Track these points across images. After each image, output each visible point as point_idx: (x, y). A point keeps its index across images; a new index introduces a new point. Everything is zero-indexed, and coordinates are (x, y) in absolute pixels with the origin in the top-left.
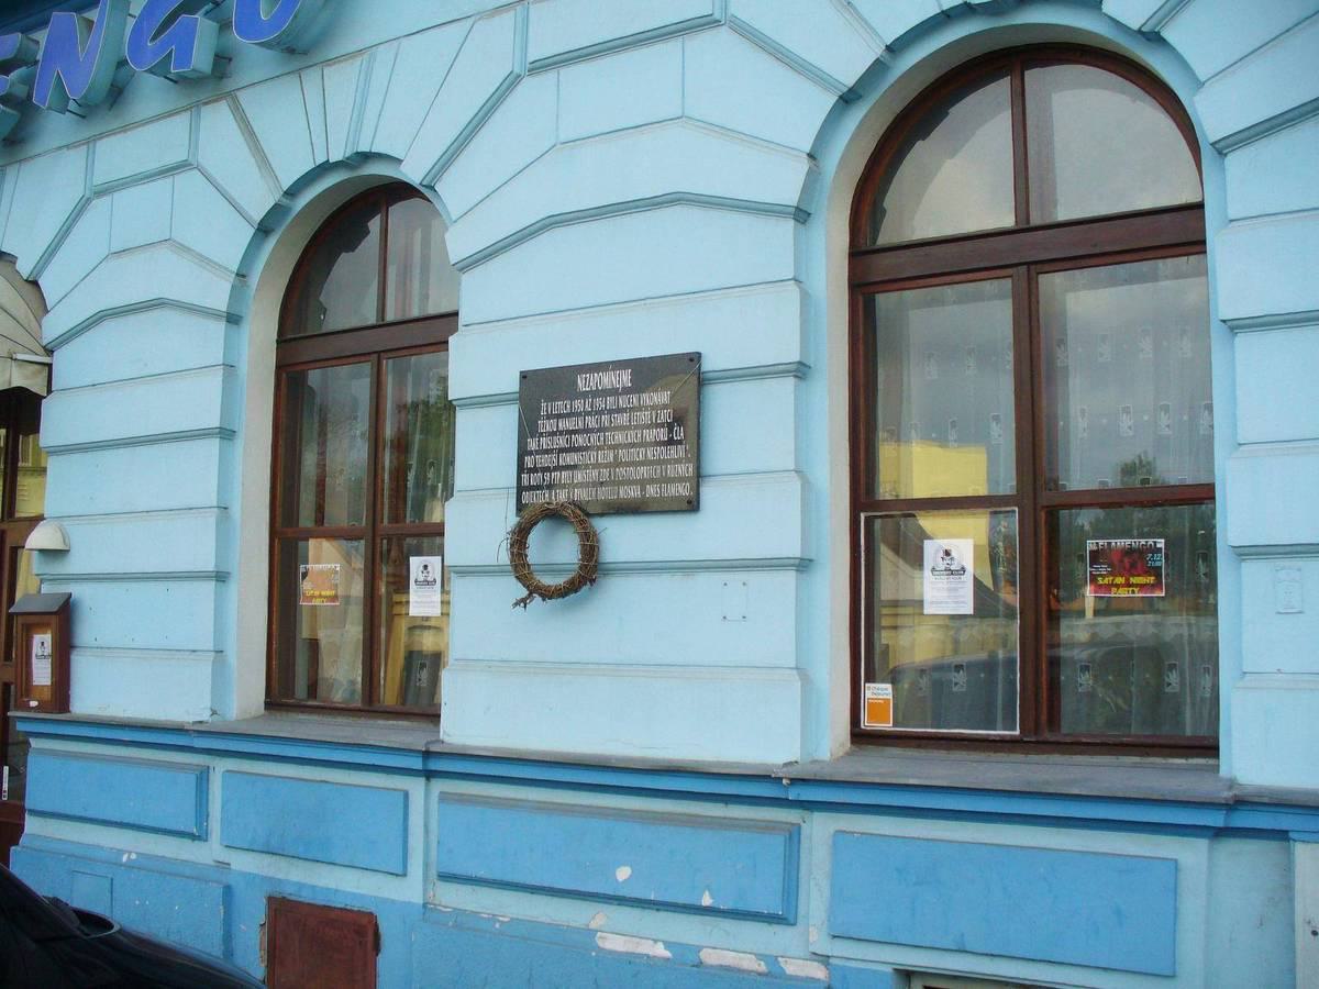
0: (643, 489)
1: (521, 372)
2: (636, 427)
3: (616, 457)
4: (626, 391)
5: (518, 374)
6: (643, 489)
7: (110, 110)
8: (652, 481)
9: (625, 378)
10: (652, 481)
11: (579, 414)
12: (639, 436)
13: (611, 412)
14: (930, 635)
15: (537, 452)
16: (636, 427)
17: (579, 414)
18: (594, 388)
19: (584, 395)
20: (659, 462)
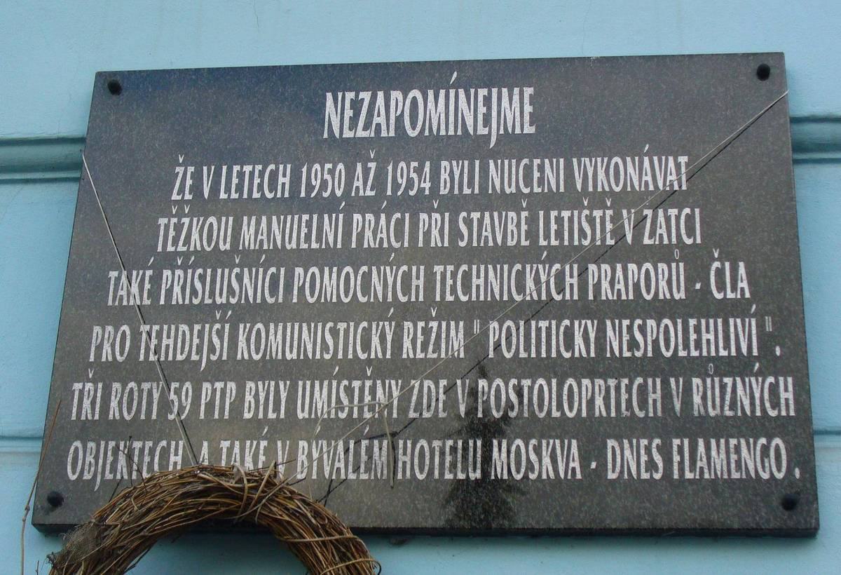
0: (593, 451)
1: (780, 56)
2: (557, 255)
3: (476, 343)
4: (512, 145)
5: (91, 80)
6: (593, 451)
7: (172, 542)
8: (627, 428)
9: (336, 114)
10: (627, 428)
11: (330, 206)
12: (572, 280)
13: (453, 204)
14: (457, 425)
15: (145, 314)
16: (557, 255)
17: (330, 206)
18: (389, 132)
19: (351, 151)
20: (658, 366)
